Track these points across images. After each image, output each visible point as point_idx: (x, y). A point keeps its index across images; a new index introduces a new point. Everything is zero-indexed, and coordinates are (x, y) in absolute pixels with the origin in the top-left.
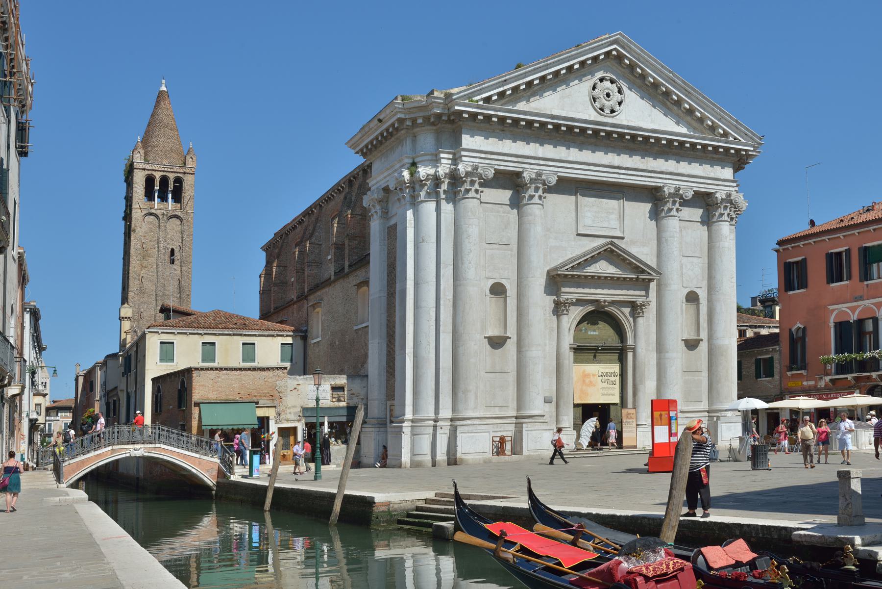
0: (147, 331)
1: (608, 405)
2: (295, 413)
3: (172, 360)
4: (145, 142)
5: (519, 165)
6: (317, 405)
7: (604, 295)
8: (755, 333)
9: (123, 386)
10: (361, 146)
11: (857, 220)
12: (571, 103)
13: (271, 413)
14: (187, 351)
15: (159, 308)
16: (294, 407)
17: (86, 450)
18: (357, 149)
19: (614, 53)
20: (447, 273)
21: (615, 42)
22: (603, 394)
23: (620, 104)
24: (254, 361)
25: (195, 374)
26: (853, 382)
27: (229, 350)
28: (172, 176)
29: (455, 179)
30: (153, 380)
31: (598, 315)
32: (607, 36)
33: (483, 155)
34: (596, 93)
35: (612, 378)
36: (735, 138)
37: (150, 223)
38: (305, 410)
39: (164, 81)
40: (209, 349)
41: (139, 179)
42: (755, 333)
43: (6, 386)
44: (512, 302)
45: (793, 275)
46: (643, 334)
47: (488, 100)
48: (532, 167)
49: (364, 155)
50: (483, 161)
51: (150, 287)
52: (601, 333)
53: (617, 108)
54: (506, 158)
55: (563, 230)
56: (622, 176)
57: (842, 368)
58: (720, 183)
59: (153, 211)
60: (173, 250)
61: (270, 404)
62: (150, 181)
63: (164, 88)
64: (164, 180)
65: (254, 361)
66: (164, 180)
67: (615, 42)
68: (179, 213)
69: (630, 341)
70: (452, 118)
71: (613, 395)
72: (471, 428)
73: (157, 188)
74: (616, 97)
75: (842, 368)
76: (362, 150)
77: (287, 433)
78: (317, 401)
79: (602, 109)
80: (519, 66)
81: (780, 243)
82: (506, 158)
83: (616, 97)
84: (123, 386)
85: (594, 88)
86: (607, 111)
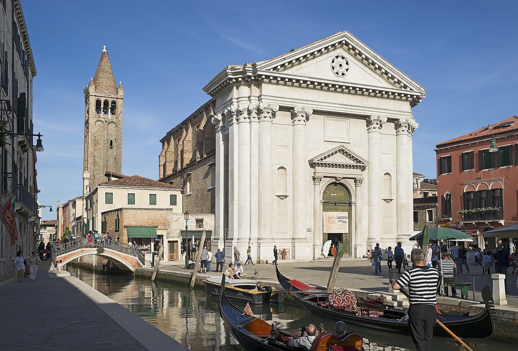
0: (98, 187)
1: (342, 234)
2: (177, 234)
3: (112, 203)
4: (95, 80)
5: (293, 104)
6: (187, 229)
7: (339, 173)
8: (433, 195)
9: (85, 215)
10: (210, 91)
11: (479, 135)
12: (320, 69)
13: (163, 233)
14: (120, 196)
15: (105, 173)
16: (177, 230)
17: (68, 250)
18: (208, 92)
19: (344, 42)
20: (255, 161)
21: (344, 36)
22: (340, 228)
23: (347, 70)
24: (155, 204)
25: (124, 211)
26: (476, 225)
27: (142, 196)
28: (110, 100)
29: (259, 111)
30: (102, 213)
31: (337, 183)
32: (340, 33)
33: (273, 98)
34: (334, 65)
35: (344, 220)
36: (411, 89)
37: (99, 126)
38: (182, 232)
39: (105, 47)
40: (131, 199)
41: (92, 101)
42: (433, 195)
43: (29, 218)
44: (290, 178)
45: (444, 165)
46: (360, 196)
47: (275, 68)
48: (300, 104)
49: (212, 96)
50: (273, 101)
51: (100, 162)
52: (337, 194)
53: (345, 72)
54: (285, 100)
55: (320, 137)
56: (348, 110)
57: (468, 216)
58: (402, 113)
59: (100, 119)
60: (111, 141)
61: (163, 227)
62: (98, 102)
63: (105, 50)
64: (106, 103)
65: (155, 204)
66: (106, 103)
67: (344, 36)
68: (114, 120)
69: (353, 200)
70: (257, 78)
71: (345, 228)
72: (268, 244)
73: (102, 106)
74: (345, 66)
75: (468, 216)
76: (211, 93)
77: (172, 243)
78: (187, 227)
79: (337, 73)
80: (292, 51)
81: (438, 146)
82: (285, 100)
83: (345, 66)
84: (85, 215)
85: (333, 62)
86: (340, 74)
